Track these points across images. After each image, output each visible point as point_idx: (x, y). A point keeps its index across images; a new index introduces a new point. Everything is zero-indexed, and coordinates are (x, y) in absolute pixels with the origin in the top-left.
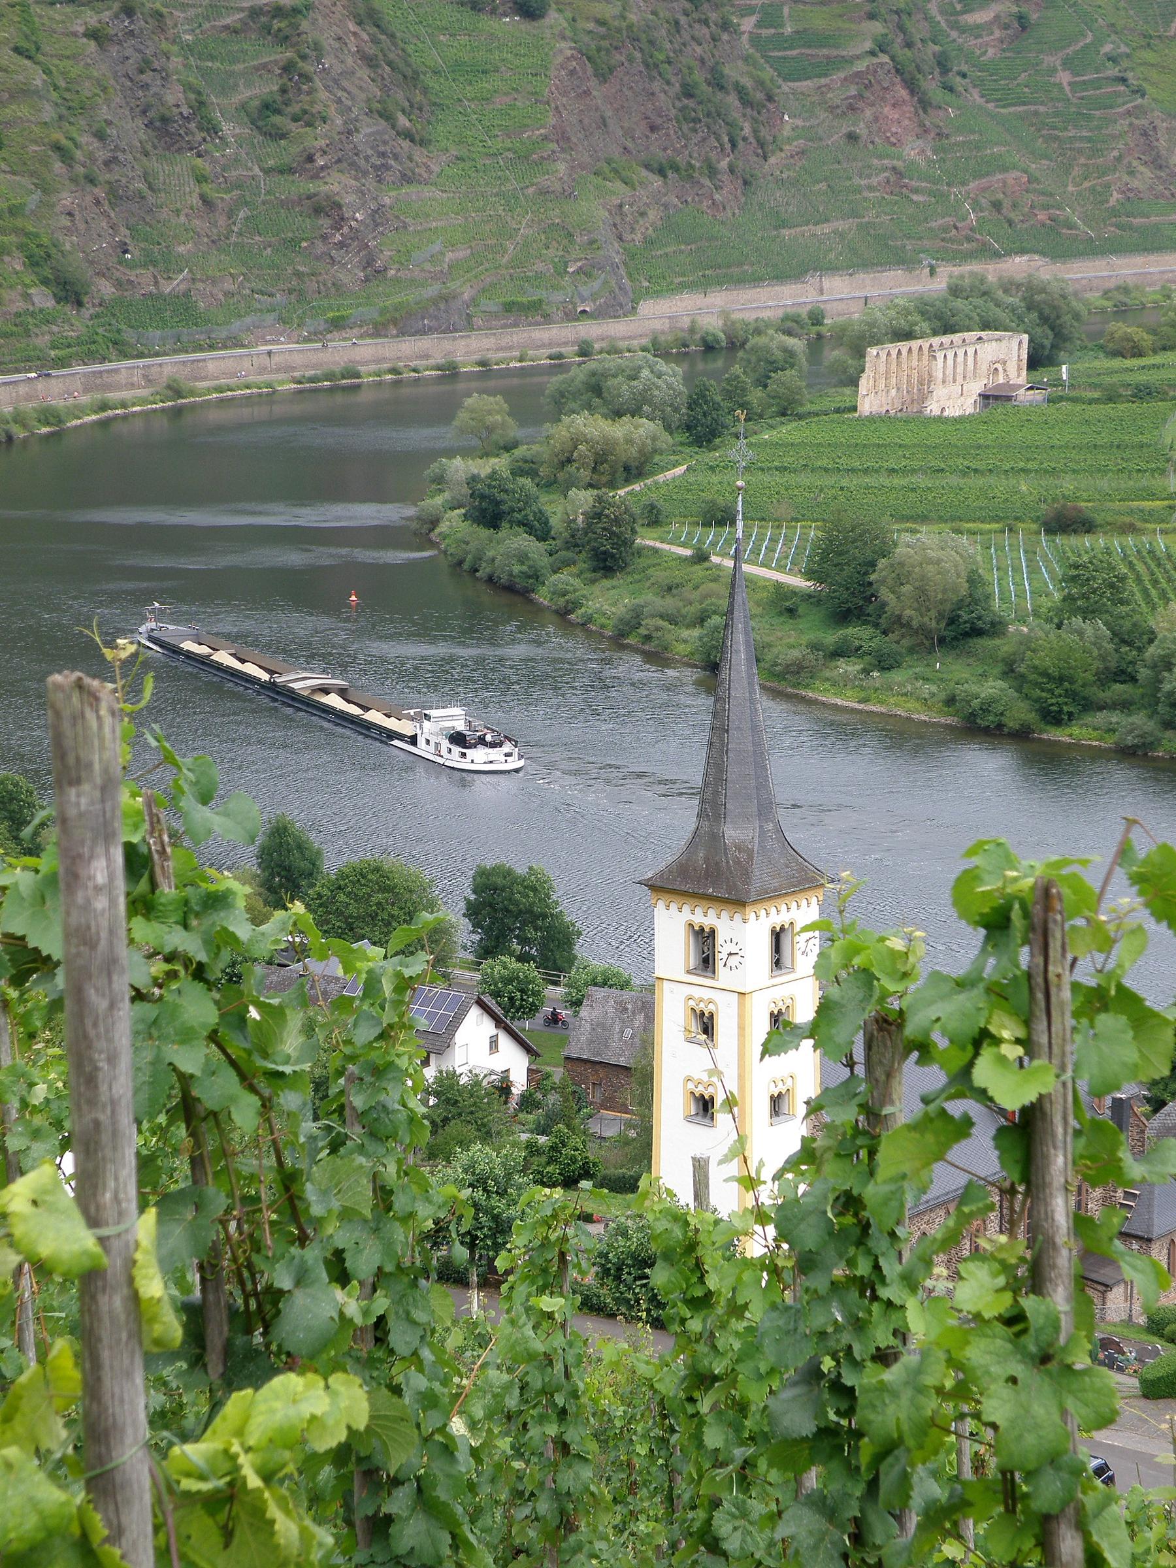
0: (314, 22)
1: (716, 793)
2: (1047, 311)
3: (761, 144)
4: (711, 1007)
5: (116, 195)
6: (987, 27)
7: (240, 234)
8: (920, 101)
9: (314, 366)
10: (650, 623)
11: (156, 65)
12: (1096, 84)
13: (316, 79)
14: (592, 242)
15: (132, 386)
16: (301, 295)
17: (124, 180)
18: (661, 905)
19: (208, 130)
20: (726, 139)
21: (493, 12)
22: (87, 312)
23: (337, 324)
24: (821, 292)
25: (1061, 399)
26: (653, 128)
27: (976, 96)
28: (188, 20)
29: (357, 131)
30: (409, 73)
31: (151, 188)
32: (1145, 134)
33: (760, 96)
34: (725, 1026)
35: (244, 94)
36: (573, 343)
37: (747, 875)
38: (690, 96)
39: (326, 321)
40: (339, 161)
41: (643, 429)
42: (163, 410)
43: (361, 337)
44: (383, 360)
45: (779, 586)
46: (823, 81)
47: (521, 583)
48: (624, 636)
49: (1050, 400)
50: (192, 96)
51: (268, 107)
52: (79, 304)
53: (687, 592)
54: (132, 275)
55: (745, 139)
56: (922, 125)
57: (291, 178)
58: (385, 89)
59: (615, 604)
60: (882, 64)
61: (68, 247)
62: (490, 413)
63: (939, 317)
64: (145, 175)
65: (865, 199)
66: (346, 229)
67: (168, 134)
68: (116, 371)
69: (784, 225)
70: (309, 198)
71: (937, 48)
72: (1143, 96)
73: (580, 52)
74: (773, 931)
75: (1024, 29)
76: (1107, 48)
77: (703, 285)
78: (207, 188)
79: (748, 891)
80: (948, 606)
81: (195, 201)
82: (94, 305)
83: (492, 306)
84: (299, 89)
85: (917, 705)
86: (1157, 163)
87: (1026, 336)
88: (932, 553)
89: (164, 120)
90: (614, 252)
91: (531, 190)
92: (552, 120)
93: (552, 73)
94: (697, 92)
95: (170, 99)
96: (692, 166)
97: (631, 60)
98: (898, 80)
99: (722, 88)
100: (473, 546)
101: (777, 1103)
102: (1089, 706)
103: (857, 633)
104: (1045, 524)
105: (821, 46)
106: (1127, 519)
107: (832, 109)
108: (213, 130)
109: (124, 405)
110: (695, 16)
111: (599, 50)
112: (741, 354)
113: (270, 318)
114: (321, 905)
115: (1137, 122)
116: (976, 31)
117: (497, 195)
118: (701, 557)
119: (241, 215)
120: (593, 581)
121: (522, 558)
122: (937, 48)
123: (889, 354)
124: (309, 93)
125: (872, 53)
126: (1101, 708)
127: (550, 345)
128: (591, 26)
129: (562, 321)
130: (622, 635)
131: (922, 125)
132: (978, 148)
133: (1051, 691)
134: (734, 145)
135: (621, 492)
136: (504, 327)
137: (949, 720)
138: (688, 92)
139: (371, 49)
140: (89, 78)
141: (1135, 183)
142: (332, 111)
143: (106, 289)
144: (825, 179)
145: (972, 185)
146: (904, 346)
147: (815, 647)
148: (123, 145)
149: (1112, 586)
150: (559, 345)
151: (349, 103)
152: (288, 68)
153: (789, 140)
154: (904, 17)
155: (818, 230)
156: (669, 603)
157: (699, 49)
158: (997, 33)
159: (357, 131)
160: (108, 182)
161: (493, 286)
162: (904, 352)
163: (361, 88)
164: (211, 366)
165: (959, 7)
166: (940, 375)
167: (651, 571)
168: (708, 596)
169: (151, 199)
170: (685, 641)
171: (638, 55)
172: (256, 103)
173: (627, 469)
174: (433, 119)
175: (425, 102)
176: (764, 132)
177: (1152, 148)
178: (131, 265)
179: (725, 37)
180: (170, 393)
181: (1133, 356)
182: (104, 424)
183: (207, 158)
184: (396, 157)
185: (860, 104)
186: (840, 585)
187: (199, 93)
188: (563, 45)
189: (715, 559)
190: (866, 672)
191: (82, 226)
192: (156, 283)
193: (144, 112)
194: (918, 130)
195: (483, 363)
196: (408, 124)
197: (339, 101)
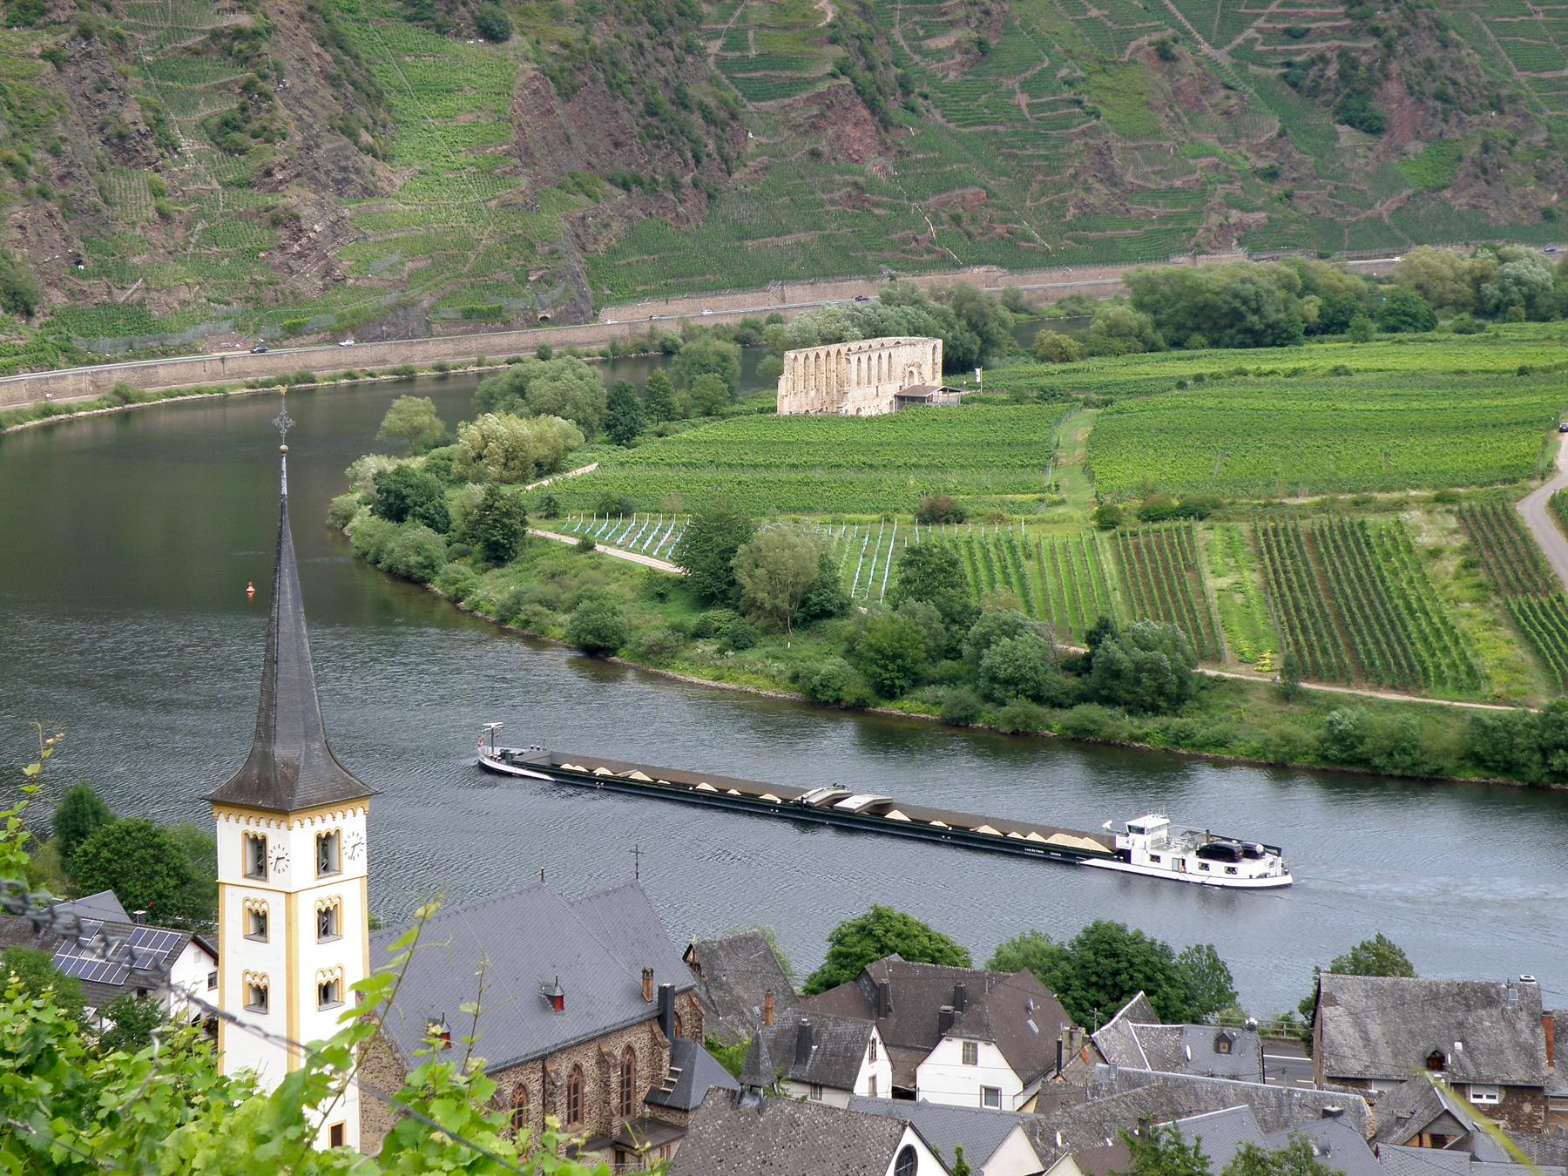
0: (276, 44)
1: (268, 717)
2: (975, 319)
3: (725, 160)
4: (264, 907)
5: (70, 208)
6: (949, 52)
7: (197, 245)
8: (881, 120)
9: (269, 372)
10: (528, 608)
11: (113, 85)
12: (1051, 106)
13: (276, 98)
14: (553, 252)
15: (80, 392)
16: (257, 302)
17: (78, 194)
18: (222, 817)
19: (166, 146)
20: (690, 155)
21: (458, 35)
22: (36, 322)
23: (294, 331)
24: (783, 300)
25: (974, 400)
26: (617, 145)
27: (938, 116)
28: (151, 43)
29: (318, 146)
30: (373, 91)
31: (106, 201)
32: (1100, 153)
33: (723, 115)
34: (275, 924)
35: (204, 112)
36: (533, 348)
37: (291, 784)
38: (653, 114)
39: (283, 328)
40: (298, 175)
41: (556, 426)
42: (110, 415)
43: (319, 343)
44: (340, 365)
45: (652, 571)
46: (787, 101)
47: (419, 573)
48: (509, 623)
49: (963, 401)
50: (150, 114)
51: (227, 124)
52: (29, 313)
53: (567, 580)
54: (84, 285)
55: (709, 155)
56: (883, 143)
57: (249, 191)
58: (348, 107)
59: (500, 592)
60: (843, 86)
61: (18, 258)
62: (417, 414)
63: (869, 323)
64: (101, 189)
65: (827, 213)
66: (304, 241)
67: (125, 149)
68: (63, 378)
69: (747, 236)
70: (267, 210)
71: (900, 71)
72: (1098, 117)
73: (543, 72)
74: (319, 838)
75: (984, 53)
76: (1064, 72)
77: (665, 293)
78: (164, 202)
79: (291, 802)
80: (800, 590)
81: (151, 213)
82: (45, 315)
83: (450, 313)
84: (259, 108)
85: (766, 682)
86: (1112, 180)
87: (939, 342)
88: (788, 538)
89: (121, 137)
90: (576, 261)
91: (494, 203)
92: (514, 137)
93: (515, 92)
94: (661, 111)
95: (127, 116)
96: (656, 181)
97: (594, 80)
98: (859, 100)
99: (686, 107)
100: (378, 536)
101: (325, 992)
102: (918, 681)
103: (718, 615)
104: (919, 515)
105: (785, 69)
106: (996, 511)
107: (795, 127)
108: (173, 147)
109: (69, 410)
110: (660, 39)
111: (562, 71)
112: (675, 358)
113: (226, 325)
114: (86, 862)
115: (1091, 142)
116: (938, 55)
117: (460, 207)
118: (586, 546)
119: (199, 227)
120: (486, 570)
121: (419, 549)
122: (900, 71)
123: (807, 357)
124: (268, 111)
125: (834, 76)
126: (930, 683)
127: (509, 350)
128: (554, 48)
129: (522, 327)
130: (504, 620)
131: (883, 143)
132: (938, 165)
133: (885, 668)
134: (698, 161)
135: (529, 488)
136: (462, 333)
137: (794, 696)
138: (651, 110)
139: (334, 70)
140: (45, 97)
141: (1092, 200)
142: (292, 127)
143: (58, 299)
144: (789, 194)
145: (932, 200)
146: (833, 348)
147: (676, 628)
148: (79, 160)
149: (942, 570)
150: (518, 350)
151: (311, 120)
152: (247, 88)
153: (753, 156)
154: (865, 42)
155: (780, 241)
156: (550, 590)
157: (663, 71)
158: (958, 58)
159: (318, 146)
160: (63, 197)
161: (454, 294)
162: (823, 356)
163: (323, 106)
164: (162, 372)
165: (921, 33)
166: (854, 377)
167: (538, 560)
168: (586, 582)
169: (107, 212)
170: (561, 625)
171: (601, 76)
172: (216, 120)
173: (539, 465)
174: (397, 136)
175: (389, 119)
176: (727, 149)
177: (1106, 166)
178: (84, 276)
179: (690, 59)
180: (118, 399)
181: (1062, 361)
182: (48, 429)
183: (165, 172)
184: (358, 171)
185: (823, 123)
186: (704, 570)
187: (157, 111)
188: (527, 66)
189: (599, 548)
190: (721, 651)
191: (34, 238)
192: (110, 293)
193: (101, 130)
194: (880, 148)
195: (440, 368)
196: (370, 140)
197: (300, 118)
